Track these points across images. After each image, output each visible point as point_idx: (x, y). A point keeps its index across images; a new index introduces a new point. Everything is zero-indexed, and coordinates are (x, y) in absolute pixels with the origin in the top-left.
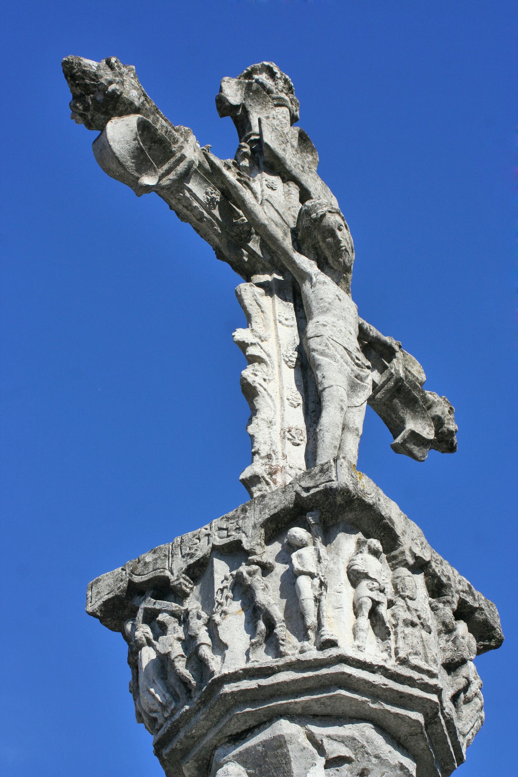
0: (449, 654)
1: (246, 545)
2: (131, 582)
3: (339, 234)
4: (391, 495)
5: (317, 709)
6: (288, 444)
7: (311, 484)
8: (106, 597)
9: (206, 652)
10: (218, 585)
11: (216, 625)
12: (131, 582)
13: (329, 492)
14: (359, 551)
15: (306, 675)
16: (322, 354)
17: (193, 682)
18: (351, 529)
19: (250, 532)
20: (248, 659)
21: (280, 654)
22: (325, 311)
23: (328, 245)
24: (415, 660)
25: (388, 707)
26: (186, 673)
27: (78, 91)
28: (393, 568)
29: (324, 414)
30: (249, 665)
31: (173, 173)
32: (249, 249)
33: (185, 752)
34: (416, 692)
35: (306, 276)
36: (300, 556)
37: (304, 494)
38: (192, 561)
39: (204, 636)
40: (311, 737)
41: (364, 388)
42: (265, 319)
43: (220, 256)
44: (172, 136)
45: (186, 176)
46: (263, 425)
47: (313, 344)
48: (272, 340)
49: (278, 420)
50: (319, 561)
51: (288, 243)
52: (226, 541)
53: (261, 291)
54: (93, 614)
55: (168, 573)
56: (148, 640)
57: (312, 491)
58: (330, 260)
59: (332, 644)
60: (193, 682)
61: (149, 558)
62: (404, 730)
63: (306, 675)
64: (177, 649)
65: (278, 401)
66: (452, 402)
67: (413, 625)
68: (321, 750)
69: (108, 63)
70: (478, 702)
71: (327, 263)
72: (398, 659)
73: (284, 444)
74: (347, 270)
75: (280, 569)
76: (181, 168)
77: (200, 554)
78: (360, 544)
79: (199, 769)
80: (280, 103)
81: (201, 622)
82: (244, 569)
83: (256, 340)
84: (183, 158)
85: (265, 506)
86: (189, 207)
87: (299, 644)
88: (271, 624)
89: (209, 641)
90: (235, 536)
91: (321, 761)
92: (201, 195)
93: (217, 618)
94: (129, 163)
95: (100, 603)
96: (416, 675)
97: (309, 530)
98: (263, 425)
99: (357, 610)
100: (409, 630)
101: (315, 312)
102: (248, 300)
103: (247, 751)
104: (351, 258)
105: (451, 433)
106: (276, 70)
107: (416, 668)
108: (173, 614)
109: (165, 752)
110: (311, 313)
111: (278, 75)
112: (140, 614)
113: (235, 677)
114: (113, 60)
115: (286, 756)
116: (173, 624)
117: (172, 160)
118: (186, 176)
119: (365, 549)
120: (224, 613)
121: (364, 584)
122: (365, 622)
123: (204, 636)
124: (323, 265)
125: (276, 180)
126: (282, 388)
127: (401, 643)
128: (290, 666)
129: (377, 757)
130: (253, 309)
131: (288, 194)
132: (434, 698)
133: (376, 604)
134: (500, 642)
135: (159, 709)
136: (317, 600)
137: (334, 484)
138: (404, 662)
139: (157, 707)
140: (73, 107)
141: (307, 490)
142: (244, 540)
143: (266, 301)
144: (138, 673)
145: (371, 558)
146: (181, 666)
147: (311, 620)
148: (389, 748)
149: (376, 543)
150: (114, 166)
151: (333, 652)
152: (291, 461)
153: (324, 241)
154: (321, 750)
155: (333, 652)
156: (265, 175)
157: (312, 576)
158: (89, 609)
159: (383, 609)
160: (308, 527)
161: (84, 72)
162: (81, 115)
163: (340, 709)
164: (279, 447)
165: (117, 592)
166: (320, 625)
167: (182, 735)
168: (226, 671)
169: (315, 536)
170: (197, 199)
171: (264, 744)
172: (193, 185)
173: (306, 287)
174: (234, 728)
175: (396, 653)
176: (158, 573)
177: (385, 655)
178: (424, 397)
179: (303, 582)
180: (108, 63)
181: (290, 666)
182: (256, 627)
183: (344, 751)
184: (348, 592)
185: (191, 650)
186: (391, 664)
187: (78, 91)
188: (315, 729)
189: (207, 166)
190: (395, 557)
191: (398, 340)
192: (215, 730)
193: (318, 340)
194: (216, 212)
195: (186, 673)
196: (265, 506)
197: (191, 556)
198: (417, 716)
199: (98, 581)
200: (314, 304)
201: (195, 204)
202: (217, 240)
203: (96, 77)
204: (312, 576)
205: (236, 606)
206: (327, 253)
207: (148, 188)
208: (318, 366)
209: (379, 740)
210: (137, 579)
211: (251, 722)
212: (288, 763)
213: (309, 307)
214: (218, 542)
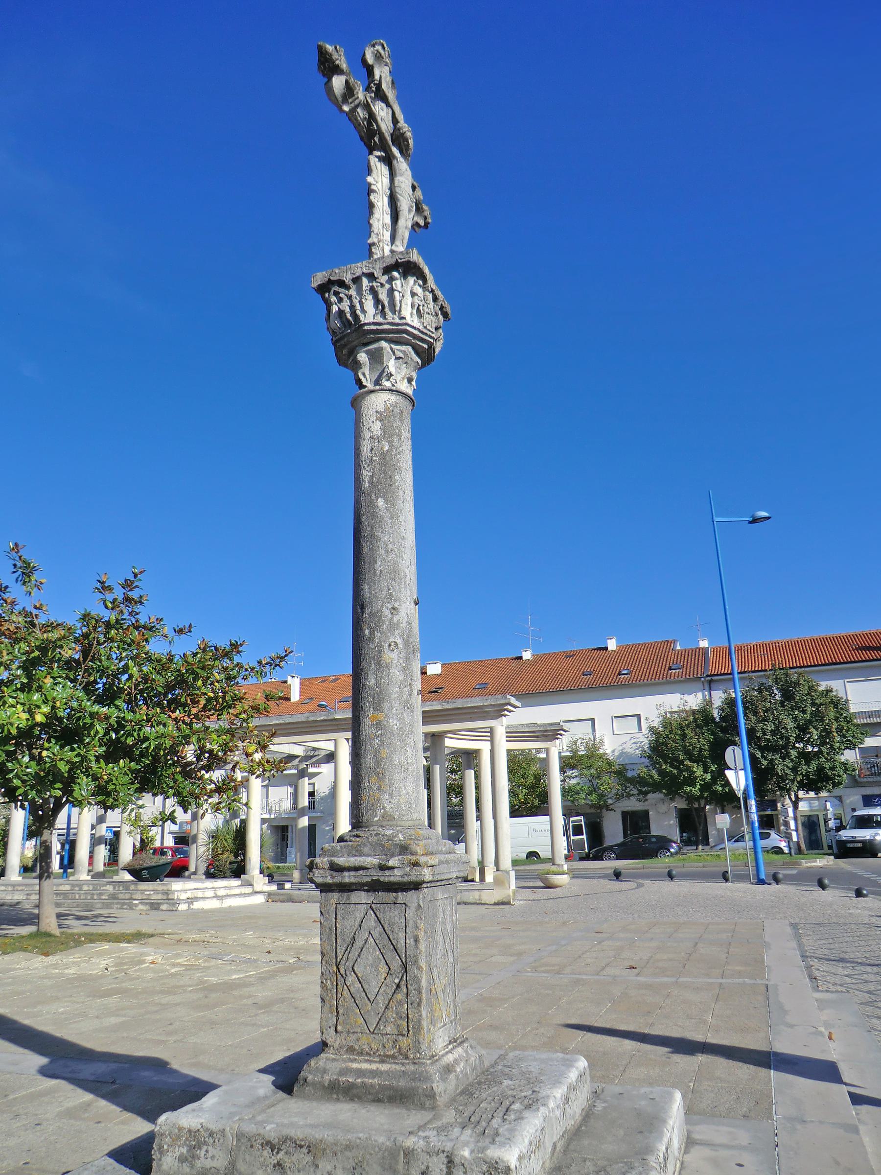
0: (436, 324)
1: (376, 275)
2: (329, 279)
3: (410, 141)
4: (427, 264)
5: (394, 339)
6: (385, 230)
7: (402, 257)
8: (319, 283)
9: (358, 312)
10: (364, 288)
11: (363, 303)
12: (329, 279)
13: (409, 262)
14: (414, 284)
15: (393, 327)
16: (401, 195)
17: (353, 323)
18: (413, 275)
19: (378, 270)
20: (374, 318)
21: (385, 318)
22: (401, 175)
23: (405, 145)
24: (429, 327)
25: (418, 342)
26: (350, 318)
27: (322, 59)
28: (424, 291)
29: (399, 221)
30: (375, 321)
31: (353, 104)
32: (374, 140)
33: (344, 346)
34: (427, 338)
35: (394, 157)
36: (395, 284)
37: (399, 261)
38: (354, 276)
39: (358, 307)
40: (391, 349)
41: (412, 211)
42: (378, 172)
43: (362, 139)
44: (354, 86)
45: (357, 106)
46: (376, 221)
47: (397, 190)
48: (380, 183)
49: (381, 219)
50: (402, 287)
51: (389, 138)
52: (369, 271)
53: (377, 160)
54: (314, 288)
55: (345, 279)
56: (336, 303)
57: (402, 260)
58: (404, 150)
59: (404, 318)
60: (353, 323)
61: (337, 271)
62: (420, 350)
63: (393, 327)
64: (347, 309)
65: (381, 211)
66: (431, 209)
67: (429, 314)
68: (394, 353)
69: (336, 48)
70: (442, 341)
71: (403, 152)
72: (423, 326)
73: (383, 230)
74: (409, 156)
75: (387, 286)
76: (357, 102)
77: (357, 274)
78: (415, 282)
79: (348, 352)
80: (386, 65)
81: (357, 301)
82: (375, 284)
83: (375, 183)
84: (358, 98)
85: (384, 262)
86: (356, 119)
87: (392, 316)
88: (383, 307)
89: (360, 309)
90: (372, 270)
91: (394, 357)
92: (361, 115)
93: (363, 301)
94: (340, 99)
95: (317, 284)
96: (428, 333)
97: (399, 274)
98: (376, 221)
99: (413, 306)
100: (427, 316)
101: (398, 175)
102: (372, 164)
103: (369, 350)
104: (411, 152)
105: (429, 223)
106: (385, 46)
107: (429, 330)
108: (346, 295)
109: (338, 344)
110: (396, 174)
111: (386, 49)
112: (332, 292)
113: (369, 324)
114: (338, 47)
115: (383, 354)
116: (345, 299)
117: (353, 98)
118: (357, 106)
119: (417, 284)
120: (366, 299)
121: (416, 297)
122: (415, 311)
123: (358, 307)
124: (401, 152)
125: (383, 105)
126: (383, 206)
127: (425, 321)
128: (388, 323)
129: (411, 358)
130: (373, 168)
131: (388, 113)
132: (432, 341)
133: (419, 305)
134: (449, 319)
135: (338, 329)
136: (401, 302)
137: (412, 260)
138: (425, 327)
139: (337, 328)
140: (319, 67)
141: (401, 259)
142: (375, 273)
143: (378, 164)
144: (330, 314)
145: (419, 288)
146: (348, 315)
147: (398, 308)
148: (415, 355)
149: (421, 282)
150: (333, 98)
151: (404, 321)
152: (385, 238)
153: (404, 143)
154: (394, 353)
155: (404, 321)
156: (380, 102)
157: (400, 292)
158: (313, 286)
159: (421, 308)
160: (399, 273)
161: (326, 51)
162: (322, 71)
163: (402, 340)
164: (381, 231)
165: (324, 282)
166: (400, 310)
167: (346, 339)
168: (366, 321)
169: (401, 277)
170: (360, 116)
171: (375, 348)
172: (359, 110)
173: (395, 162)
174: (366, 341)
175: (423, 324)
176: (341, 278)
177: (419, 324)
178: (422, 207)
179: (396, 293)
180: (336, 48)
181: (388, 323)
182: (378, 307)
183: (401, 355)
184: (410, 299)
185: (352, 310)
186: (421, 328)
187: (322, 59)
188: (393, 346)
189: (365, 102)
190: (425, 288)
191: (417, 182)
192: (357, 341)
193: (399, 188)
194: (365, 123)
195: (350, 318)
196: (384, 262)
197: (354, 274)
198: (426, 346)
199: (316, 275)
200: (397, 171)
201: (359, 119)
202: (363, 134)
203: (331, 55)
204: (400, 292)
205: (370, 297)
206: (404, 148)
207: (344, 112)
208: (398, 200)
209: (412, 352)
210: (332, 278)
211: (371, 340)
212: (383, 357)
213: (395, 172)
214: (365, 271)
